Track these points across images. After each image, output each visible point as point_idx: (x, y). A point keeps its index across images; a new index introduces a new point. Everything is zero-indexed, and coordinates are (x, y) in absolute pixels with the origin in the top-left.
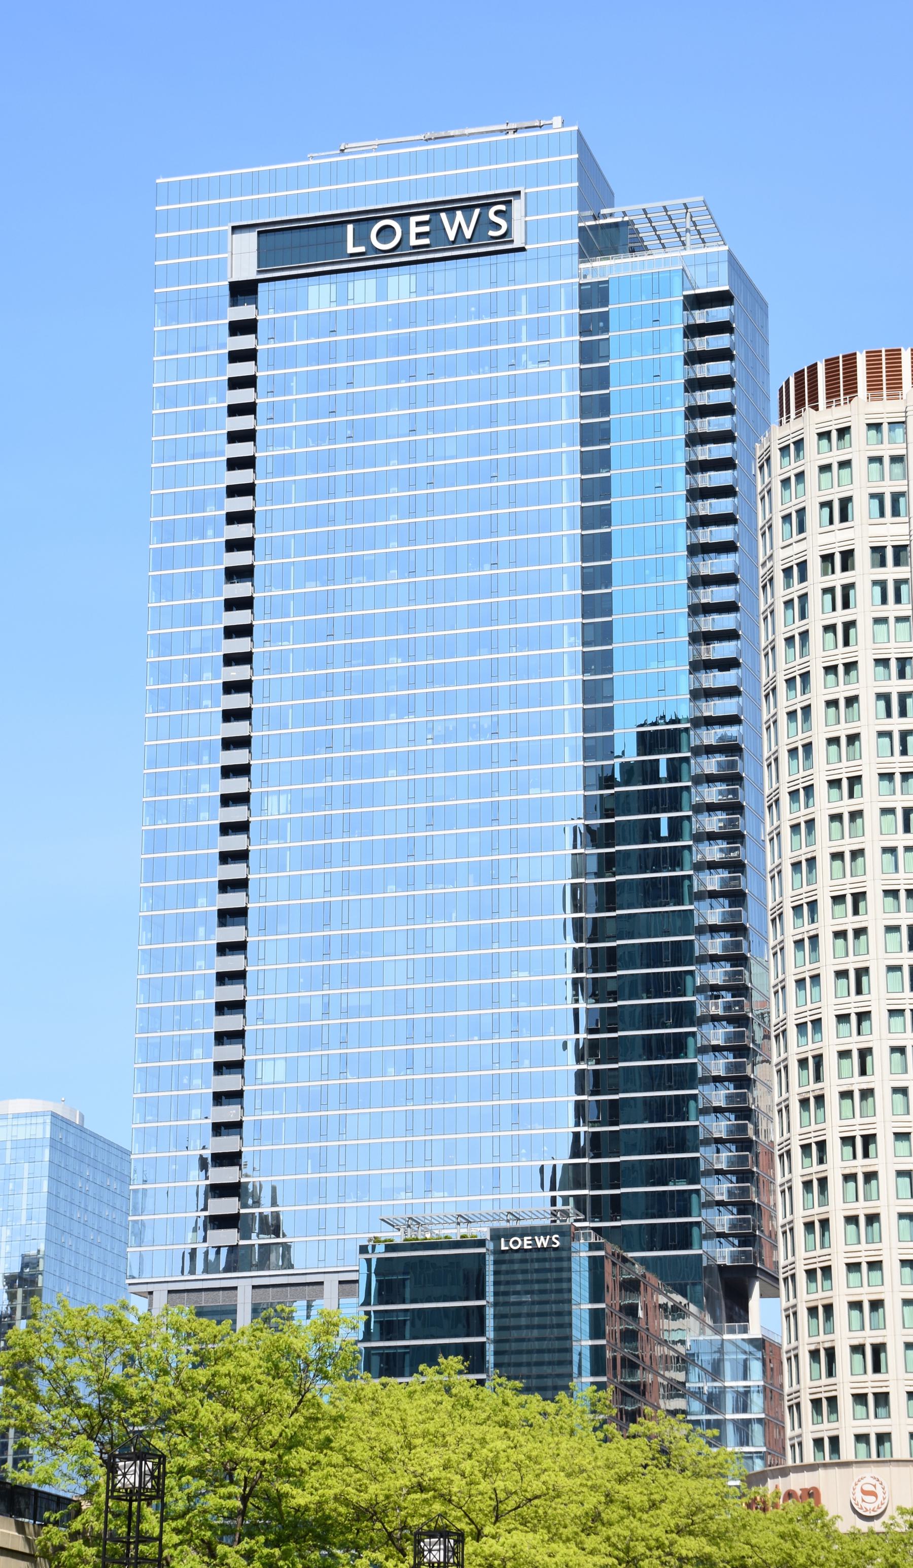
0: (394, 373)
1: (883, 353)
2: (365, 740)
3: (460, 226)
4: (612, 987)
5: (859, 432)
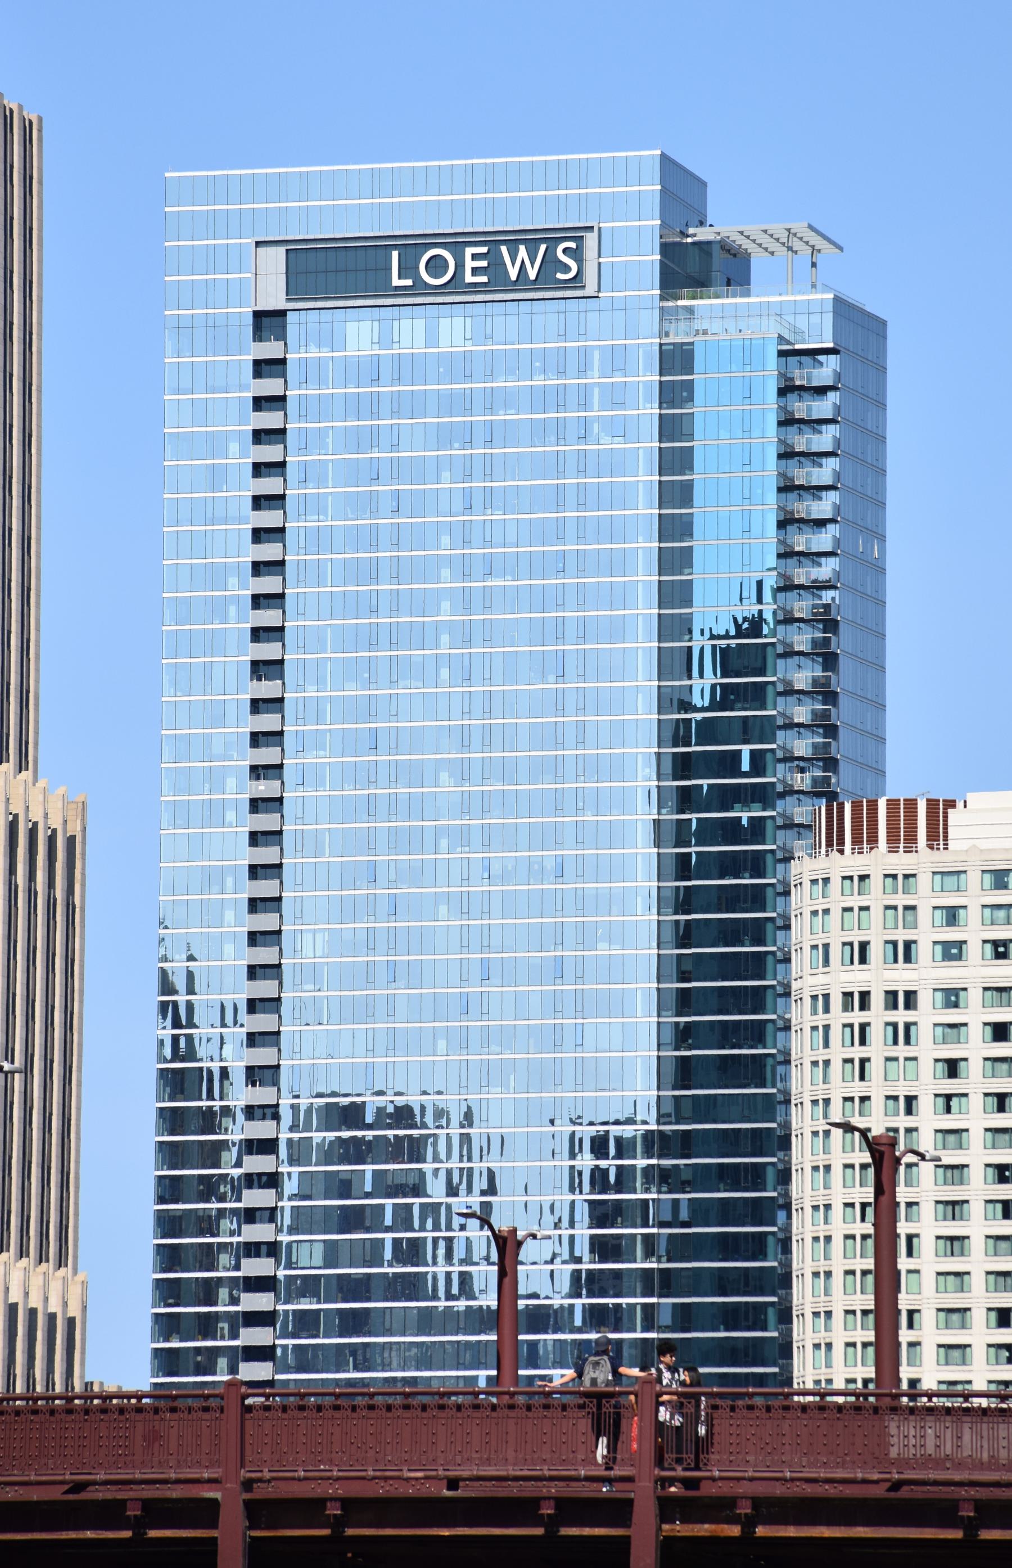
0: (445, 436)
1: (902, 802)
2: (413, 875)
3: (523, 262)
4: (685, 1176)
5: (876, 882)
